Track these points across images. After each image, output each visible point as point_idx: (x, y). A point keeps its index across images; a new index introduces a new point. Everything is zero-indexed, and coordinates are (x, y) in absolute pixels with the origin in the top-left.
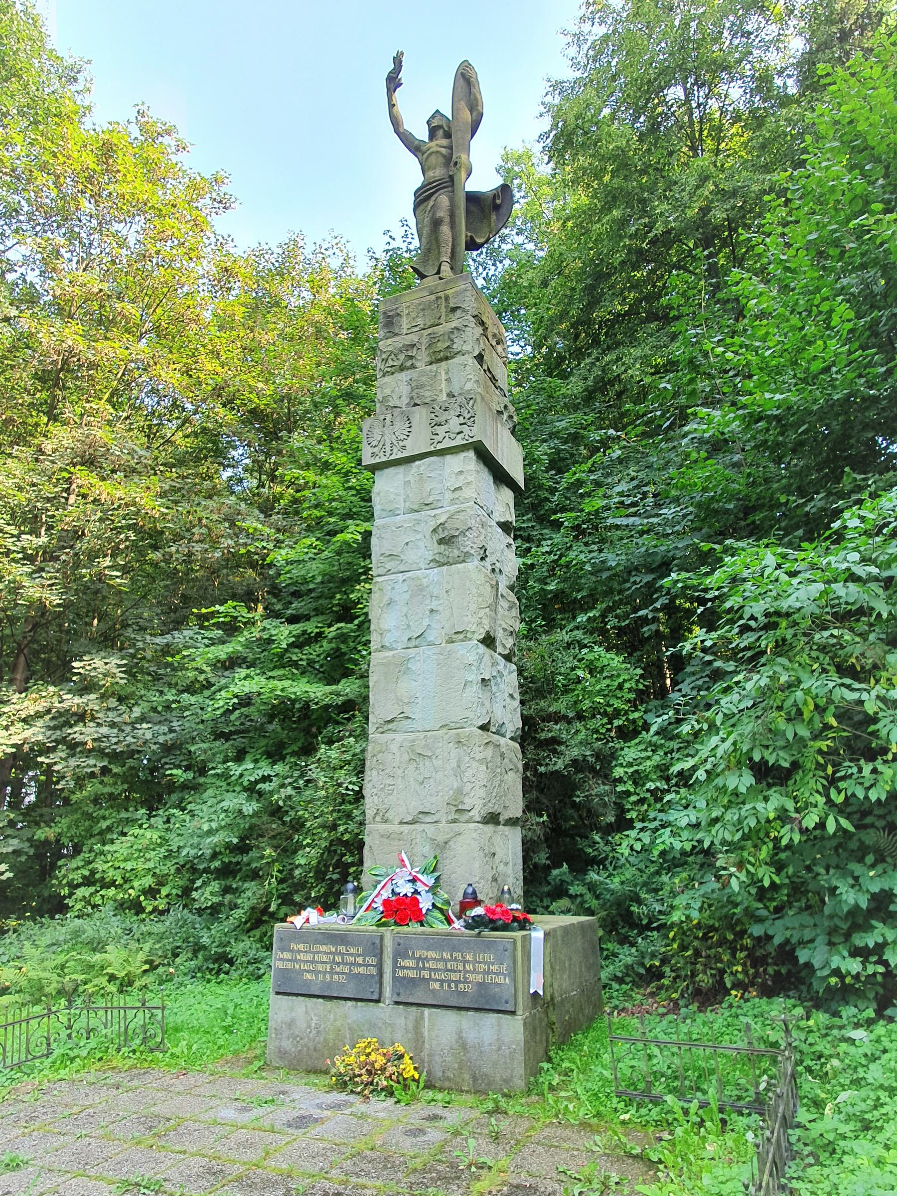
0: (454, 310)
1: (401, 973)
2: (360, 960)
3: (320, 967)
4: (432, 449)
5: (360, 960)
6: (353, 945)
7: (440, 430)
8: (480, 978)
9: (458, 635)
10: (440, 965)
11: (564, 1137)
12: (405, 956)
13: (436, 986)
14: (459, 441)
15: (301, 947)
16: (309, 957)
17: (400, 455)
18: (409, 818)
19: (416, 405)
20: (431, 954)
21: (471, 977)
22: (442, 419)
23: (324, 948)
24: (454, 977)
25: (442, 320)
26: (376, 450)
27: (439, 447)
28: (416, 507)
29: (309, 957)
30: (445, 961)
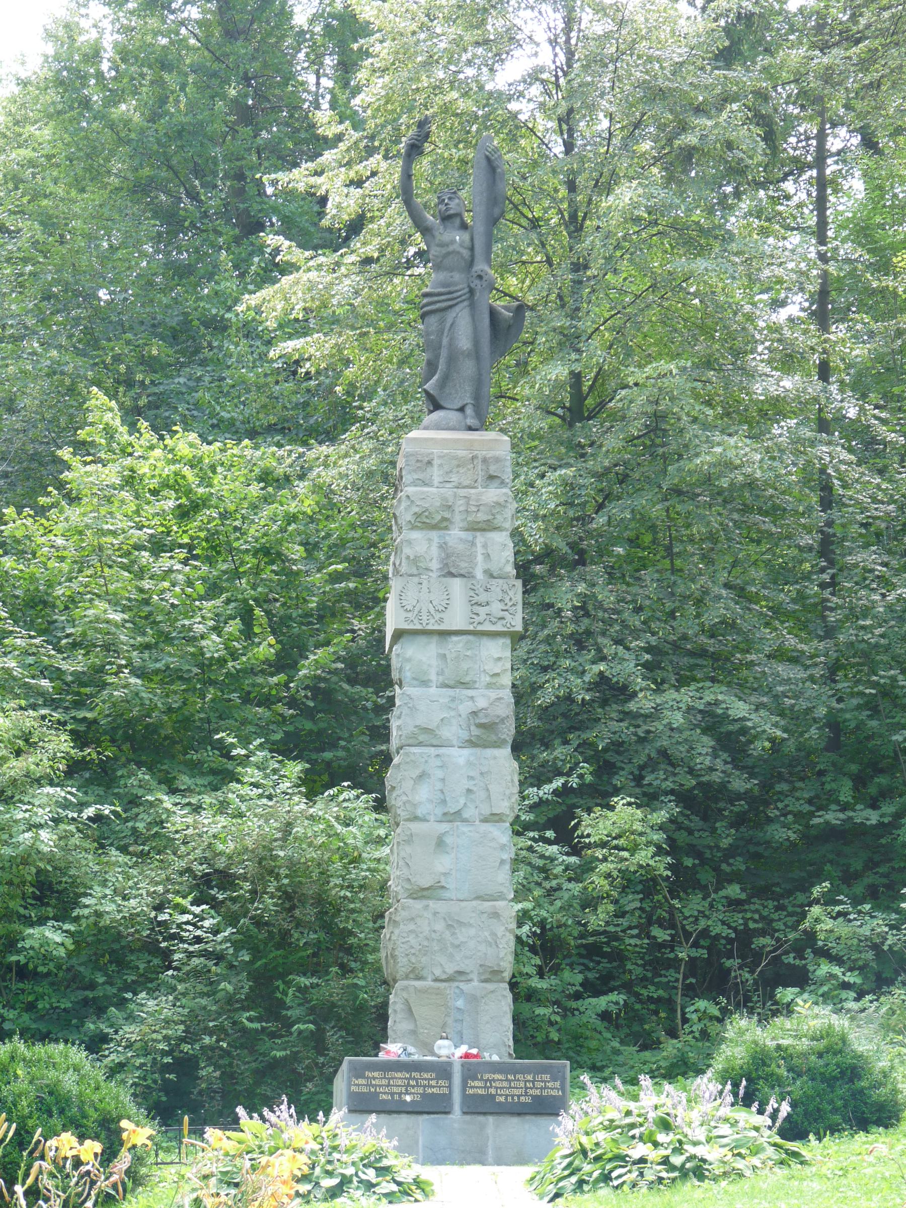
0: (491, 478)
1: (471, 1092)
2: (433, 1083)
3: (395, 1090)
4: (471, 628)
5: (433, 1083)
6: (427, 1071)
7: (482, 611)
8: (538, 1092)
9: (492, 975)
10: (505, 1084)
11: (33, 56)
12: (475, 1078)
13: (502, 1099)
14: (499, 627)
15: (376, 1074)
16: (385, 1082)
17: (436, 627)
18: (444, 977)
19: (452, 575)
20: (497, 1076)
21: (531, 1092)
22: (483, 598)
23: (399, 1075)
24: (516, 1092)
25: (478, 484)
26: (409, 615)
27: (480, 628)
28: (452, 683)
29: (385, 1082)
30: (510, 1081)
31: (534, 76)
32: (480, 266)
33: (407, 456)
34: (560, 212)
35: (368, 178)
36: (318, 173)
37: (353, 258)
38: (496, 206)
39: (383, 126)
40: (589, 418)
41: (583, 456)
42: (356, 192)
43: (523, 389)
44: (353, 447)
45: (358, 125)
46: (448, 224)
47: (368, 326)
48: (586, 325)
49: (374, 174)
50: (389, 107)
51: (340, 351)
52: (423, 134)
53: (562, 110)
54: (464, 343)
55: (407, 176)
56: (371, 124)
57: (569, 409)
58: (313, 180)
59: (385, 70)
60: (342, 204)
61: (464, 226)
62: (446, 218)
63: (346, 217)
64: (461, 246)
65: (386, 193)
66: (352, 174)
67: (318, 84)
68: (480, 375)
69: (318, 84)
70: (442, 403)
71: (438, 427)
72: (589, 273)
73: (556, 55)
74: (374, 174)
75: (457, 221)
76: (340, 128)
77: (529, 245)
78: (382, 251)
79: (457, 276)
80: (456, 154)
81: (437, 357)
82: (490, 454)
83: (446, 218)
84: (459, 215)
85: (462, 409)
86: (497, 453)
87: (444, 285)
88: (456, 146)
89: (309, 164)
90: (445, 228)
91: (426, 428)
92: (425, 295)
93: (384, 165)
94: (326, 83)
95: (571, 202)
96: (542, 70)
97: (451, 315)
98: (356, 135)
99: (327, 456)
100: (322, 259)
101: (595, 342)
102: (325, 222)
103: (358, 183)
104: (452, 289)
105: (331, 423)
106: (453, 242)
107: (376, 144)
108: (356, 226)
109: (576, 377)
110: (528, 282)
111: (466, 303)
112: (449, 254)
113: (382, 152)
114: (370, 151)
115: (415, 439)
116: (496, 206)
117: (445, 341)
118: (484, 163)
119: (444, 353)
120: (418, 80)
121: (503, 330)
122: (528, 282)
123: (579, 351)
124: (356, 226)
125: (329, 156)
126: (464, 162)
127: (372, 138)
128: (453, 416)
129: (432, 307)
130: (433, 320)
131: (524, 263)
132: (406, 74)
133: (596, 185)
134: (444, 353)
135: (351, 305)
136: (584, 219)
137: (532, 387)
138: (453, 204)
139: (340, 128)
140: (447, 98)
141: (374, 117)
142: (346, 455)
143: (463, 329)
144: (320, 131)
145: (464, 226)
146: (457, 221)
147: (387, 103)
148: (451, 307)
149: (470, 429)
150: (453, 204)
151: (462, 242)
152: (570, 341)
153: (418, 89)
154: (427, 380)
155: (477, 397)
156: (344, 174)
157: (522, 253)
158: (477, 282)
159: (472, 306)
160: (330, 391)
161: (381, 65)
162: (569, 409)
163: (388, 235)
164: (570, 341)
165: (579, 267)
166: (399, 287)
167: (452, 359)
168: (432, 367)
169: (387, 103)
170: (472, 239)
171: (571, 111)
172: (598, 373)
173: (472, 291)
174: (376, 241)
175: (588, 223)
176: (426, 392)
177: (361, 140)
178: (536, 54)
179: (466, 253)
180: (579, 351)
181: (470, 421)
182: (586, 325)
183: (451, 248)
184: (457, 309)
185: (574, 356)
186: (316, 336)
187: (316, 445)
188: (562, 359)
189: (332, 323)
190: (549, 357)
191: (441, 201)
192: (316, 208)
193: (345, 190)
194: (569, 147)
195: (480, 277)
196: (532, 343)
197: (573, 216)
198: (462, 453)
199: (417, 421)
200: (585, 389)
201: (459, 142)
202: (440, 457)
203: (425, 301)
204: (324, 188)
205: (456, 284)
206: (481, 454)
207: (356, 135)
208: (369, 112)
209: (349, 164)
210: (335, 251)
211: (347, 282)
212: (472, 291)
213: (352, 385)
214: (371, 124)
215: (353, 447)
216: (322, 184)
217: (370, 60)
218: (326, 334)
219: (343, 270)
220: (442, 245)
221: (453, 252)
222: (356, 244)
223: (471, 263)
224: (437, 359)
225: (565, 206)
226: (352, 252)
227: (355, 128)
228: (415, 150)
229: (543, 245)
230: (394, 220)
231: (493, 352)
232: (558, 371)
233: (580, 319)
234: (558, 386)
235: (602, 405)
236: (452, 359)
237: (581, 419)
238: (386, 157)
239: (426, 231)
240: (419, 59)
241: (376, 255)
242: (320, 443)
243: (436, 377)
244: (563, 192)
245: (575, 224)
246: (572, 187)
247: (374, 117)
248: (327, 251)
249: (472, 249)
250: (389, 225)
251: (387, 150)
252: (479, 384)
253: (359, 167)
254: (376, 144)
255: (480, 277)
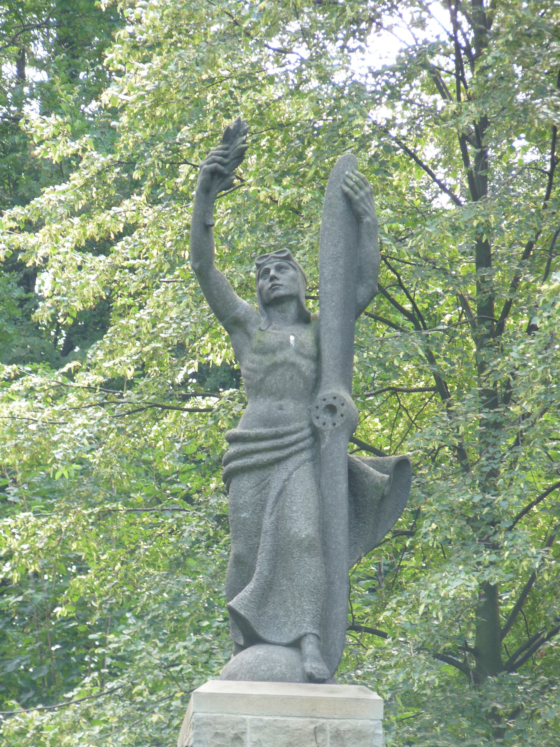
31: (416, 63)
32: (333, 389)
33: (198, 725)
34: (463, 301)
35: (119, 237)
36: (31, 227)
37: (86, 379)
38: (363, 285)
39: (150, 143)
40: (512, 667)
41: (499, 733)
42: (101, 262)
43: (395, 614)
44: (86, 714)
45: (106, 138)
46: (274, 312)
47: (113, 500)
48: (509, 501)
49: (129, 229)
50: (159, 111)
51: (64, 543)
52: (232, 152)
53: (467, 122)
54: (303, 526)
55: (203, 227)
56: (127, 141)
57: (475, 652)
58: (19, 239)
59: (156, 45)
60: (66, 281)
61: (304, 318)
62: (271, 303)
63: (78, 306)
64: (298, 352)
65: (151, 263)
66: (91, 229)
67: (21, 75)
68: (330, 583)
69: (21, 75)
70: (261, 633)
71: (254, 675)
72: (515, 409)
73: (457, 26)
74: (129, 229)
75: (292, 309)
76: (74, 146)
77: (408, 358)
78: (142, 369)
79: (290, 407)
80: (284, 193)
81: (254, 550)
82: (347, 725)
83: (271, 303)
84: (293, 297)
85: (296, 644)
86: (359, 723)
87: (266, 422)
88: (278, 182)
89: (17, 209)
90: (270, 320)
91: (231, 677)
92: (233, 440)
93: (149, 214)
94: (34, 75)
95: (481, 285)
96: (433, 49)
97: (277, 477)
98: (102, 160)
99: (39, 729)
100: (35, 380)
101: (524, 531)
102: (42, 314)
103: (100, 246)
104: (281, 429)
105: (45, 671)
106: (284, 345)
107: (136, 175)
108: (94, 323)
109: (489, 592)
110: (401, 427)
111: (305, 456)
112: (275, 366)
113: (146, 189)
114: (128, 188)
115: (211, 696)
116: (363, 285)
117: (268, 522)
118: (341, 205)
119: (265, 543)
120: (213, 64)
121: (373, 503)
122: (401, 427)
123: (495, 547)
124: (94, 323)
125: (50, 197)
126: (294, 210)
127: (129, 165)
128: (282, 657)
129: (244, 463)
130: (245, 484)
131: (395, 391)
132: (192, 53)
133: (526, 255)
134: (265, 543)
135: (81, 462)
136: (505, 314)
137: (413, 610)
138: (284, 279)
139: (74, 146)
140: (262, 98)
141: (131, 128)
142: (74, 728)
143: (300, 500)
144: (37, 151)
145: (304, 318)
146: (292, 309)
147: (156, 104)
148: (278, 461)
149: (311, 679)
150: (284, 279)
151: (300, 345)
152: (483, 529)
153: (211, 80)
154: (233, 592)
155: (324, 623)
156: (78, 230)
157: (396, 372)
158: (326, 417)
159: (317, 460)
160: (44, 613)
161: (149, 36)
162: (475, 652)
163: (155, 337)
164: (483, 529)
165: (497, 398)
166: (168, 432)
167: (280, 554)
168: (243, 568)
169: (156, 104)
170: (318, 341)
171: (483, 123)
172: (527, 589)
173: (316, 434)
174: (132, 349)
175: (510, 321)
176: (231, 610)
177: (108, 169)
178: (421, 23)
179: (306, 366)
180: (495, 547)
181: (312, 666)
182: (509, 501)
183: (280, 357)
184: (290, 465)
185: (487, 556)
186: (21, 516)
187: (18, 708)
188: (465, 561)
189: (48, 494)
190: (440, 557)
191: (263, 273)
192: (19, 293)
193: (78, 258)
194: (477, 188)
195: (332, 409)
196: (410, 534)
197: (486, 310)
198: (296, 722)
199: (206, 666)
200: (503, 620)
201: (284, 174)
202: (257, 729)
203: (233, 449)
204: (41, 252)
205: (286, 421)
206: (330, 724)
207: (102, 160)
208: (124, 119)
209: (87, 211)
210: (56, 366)
211: (80, 419)
212: (316, 434)
213: (82, 604)
214: (127, 141)
215: (86, 714)
216: (38, 243)
217: (129, 29)
218: (38, 514)
219: (72, 399)
220: (264, 351)
221: (283, 364)
222: (96, 353)
223: (316, 383)
224: (251, 552)
225: (471, 290)
226: (92, 366)
227: (98, 144)
228: (218, 178)
229: (432, 359)
230: (168, 308)
231: (352, 544)
232: (458, 583)
233: (497, 491)
234: (457, 607)
235: (532, 645)
236: (280, 554)
237: (497, 667)
238: (153, 201)
239: (235, 324)
240: (215, 28)
241: (130, 374)
242: (25, 706)
243: (250, 587)
244: (466, 266)
245: (488, 321)
246: (484, 256)
247: (131, 128)
248: (40, 367)
249: (317, 358)
250: (155, 320)
251: (156, 186)
252: (326, 600)
253: (104, 217)
254: (136, 175)
255: (332, 409)
